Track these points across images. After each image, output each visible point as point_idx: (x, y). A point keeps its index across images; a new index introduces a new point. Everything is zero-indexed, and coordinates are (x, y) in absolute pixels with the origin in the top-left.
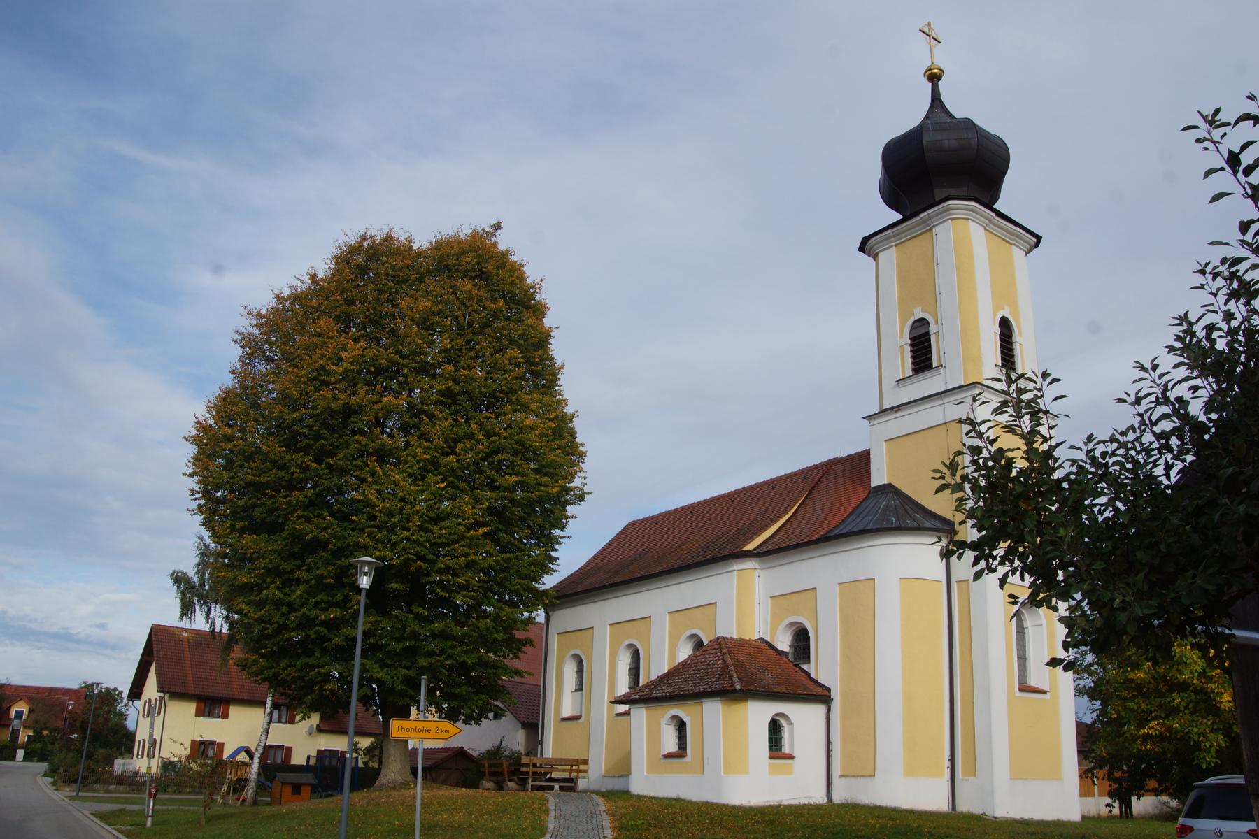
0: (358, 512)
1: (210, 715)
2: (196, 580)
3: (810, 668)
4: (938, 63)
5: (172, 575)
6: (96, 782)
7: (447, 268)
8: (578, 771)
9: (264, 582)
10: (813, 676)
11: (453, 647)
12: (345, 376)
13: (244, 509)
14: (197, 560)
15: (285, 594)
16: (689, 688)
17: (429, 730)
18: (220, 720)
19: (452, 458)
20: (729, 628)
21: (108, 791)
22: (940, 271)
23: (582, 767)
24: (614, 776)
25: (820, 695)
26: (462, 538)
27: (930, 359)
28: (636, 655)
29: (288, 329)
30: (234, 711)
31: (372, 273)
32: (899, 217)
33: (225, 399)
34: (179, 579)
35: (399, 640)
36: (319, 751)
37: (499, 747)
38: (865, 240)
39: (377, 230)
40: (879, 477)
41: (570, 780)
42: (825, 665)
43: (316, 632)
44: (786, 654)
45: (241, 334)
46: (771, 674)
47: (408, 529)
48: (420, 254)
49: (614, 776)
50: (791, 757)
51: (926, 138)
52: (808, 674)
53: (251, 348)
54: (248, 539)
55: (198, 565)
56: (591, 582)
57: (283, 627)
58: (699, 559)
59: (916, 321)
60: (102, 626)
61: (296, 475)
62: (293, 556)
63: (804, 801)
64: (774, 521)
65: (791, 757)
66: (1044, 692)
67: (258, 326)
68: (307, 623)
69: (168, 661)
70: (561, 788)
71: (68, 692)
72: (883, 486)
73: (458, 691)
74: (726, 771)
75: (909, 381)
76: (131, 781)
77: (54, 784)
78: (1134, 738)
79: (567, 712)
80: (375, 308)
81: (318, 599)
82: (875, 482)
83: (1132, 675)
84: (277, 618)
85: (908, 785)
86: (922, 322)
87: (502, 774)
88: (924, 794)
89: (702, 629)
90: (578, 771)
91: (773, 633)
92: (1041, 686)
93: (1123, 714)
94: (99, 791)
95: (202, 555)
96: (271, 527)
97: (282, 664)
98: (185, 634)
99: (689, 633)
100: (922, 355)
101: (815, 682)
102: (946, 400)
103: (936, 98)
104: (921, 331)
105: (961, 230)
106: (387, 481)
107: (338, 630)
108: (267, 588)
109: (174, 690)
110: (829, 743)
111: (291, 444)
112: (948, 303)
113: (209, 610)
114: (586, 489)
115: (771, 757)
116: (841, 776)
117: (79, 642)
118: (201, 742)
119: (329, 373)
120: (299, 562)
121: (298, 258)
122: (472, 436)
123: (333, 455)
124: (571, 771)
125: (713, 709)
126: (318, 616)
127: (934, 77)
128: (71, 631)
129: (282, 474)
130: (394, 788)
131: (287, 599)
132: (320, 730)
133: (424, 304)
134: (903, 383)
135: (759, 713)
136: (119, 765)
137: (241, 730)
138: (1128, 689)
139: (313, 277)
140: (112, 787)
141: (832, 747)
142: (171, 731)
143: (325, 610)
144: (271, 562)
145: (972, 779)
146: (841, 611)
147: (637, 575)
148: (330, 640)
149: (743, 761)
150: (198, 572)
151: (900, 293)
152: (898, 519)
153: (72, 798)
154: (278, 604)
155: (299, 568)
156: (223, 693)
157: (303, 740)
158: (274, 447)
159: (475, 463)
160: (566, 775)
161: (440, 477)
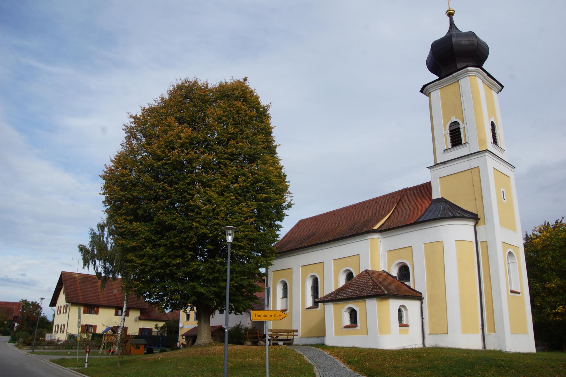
0: (193, 211)
1: (90, 313)
2: (90, 249)
3: (411, 284)
4: (452, 8)
5: (79, 247)
6: (39, 345)
7: (227, 96)
8: (294, 335)
9: (144, 245)
10: (412, 287)
11: (236, 277)
12: (182, 145)
13: (132, 210)
14: (90, 240)
15: (154, 251)
16: (357, 293)
17: (271, 316)
18: (95, 315)
19: (236, 185)
20: (366, 265)
21: (44, 349)
22: (464, 99)
23: (295, 333)
24: (307, 337)
25: (417, 296)
26: (242, 223)
27: (461, 140)
28: (316, 281)
29: (148, 125)
30: (101, 311)
31: (188, 101)
32: (437, 78)
33: (120, 157)
34: (82, 249)
35: (211, 274)
36: (140, 329)
37: (239, 325)
38: (425, 86)
39: (192, 79)
40: (436, 195)
41: (287, 340)
42: (418, 281)
43: (170, 270)
44: (396, 277)
45: (126, 126)
46: (396, 286)
47: (217, 219)
48: (211, 91)
49: (307, 337)
50: (407, 326)
51: (454, 40)
52: (409, 287)
53: (131, 134)
54: (135, 225)
55: (91, 242)
56: (289, 247)
57: (153, 268)
58: (349, 234)
59: (452, 123)
60: (23, 275)
61: (160, 193)
62: (157, 233)
63: (414, 347)
64: (384, 216)
65: (407, 326)
66: (519, 293)
67: (135, 123)
68: (166, 265)
69: (70, 288)
70: (284, 344)
71: (14, 304)
72: (439, 198)
73: (237, 298)
74: (380, 333)
75: (451, 150)
76: (54, 344)
77: (17, 346)
78: (549, 315)
79: (279, 308)
80: (193, 114)
81: (170, 253)
82: (434, 197)
83: (547, 286)
84: (150, 263)
85: (463, 337)
86: (456, 123)
87: (257, 337)
88: (471, 341)
89: (352, 267)
90: (294, 335)
91: (389, 267)
92: (517, 291)
93: (542, 303)
94: (40, 349)
95: (92, 237)
96: (147, 218)
97: (152, 286)
98: (77, 276)
99: (345, 269)
100: (456, 137)
101: (414, 290)
102: (470, 158)
103: (452, 24)
104: (456, 127)
105: (470, 82)
106: (195, 198)
107: (180, 269)
108: (146, 248)
109: (72, 301)
110: (422, 318)
111: (123, 189)
112: (469, 113)
113: (95, 263)
114: (292, 202)
115: (400, 326)
116: (429, 334)
117: (13, 282)
118: (86, 325)
119: (174, 143)
120: (160, 236)
121: (152, 89)
122: (244, 175)
123: (177, 184)
124: (288, 336)
125: (372, 305)
126: (171, 262)
127: (450, 15)
128: (9, 277)
129: (152, 192)
130: (205, 346)
131: (155, 254)
132: (140, 319)
133: (220, 112)
134: (446, 151)
135: (394, 304)
136: (48, 337)
137: (104, 320)
138: (544, 292)
139: (162, 99)
140: (46, 347)
141: (424, 320)
142: (68, 322)
143: (174, 259)
144: (147, 236)
145: (493, 334)
146: (426, 255)
147: (315, 242)
148: (176, 274)
149: (390, 329)
150: (90, 246)
151: (443, 111)
152: (452, 213)
153: (31, 353)
154: (150, 257)
155: (160, 239)
156: (94, 302)
157: (133, 324)
158: (147, 178)
159: (247, 188)
160: (285, 337)
161: (232, 194)
